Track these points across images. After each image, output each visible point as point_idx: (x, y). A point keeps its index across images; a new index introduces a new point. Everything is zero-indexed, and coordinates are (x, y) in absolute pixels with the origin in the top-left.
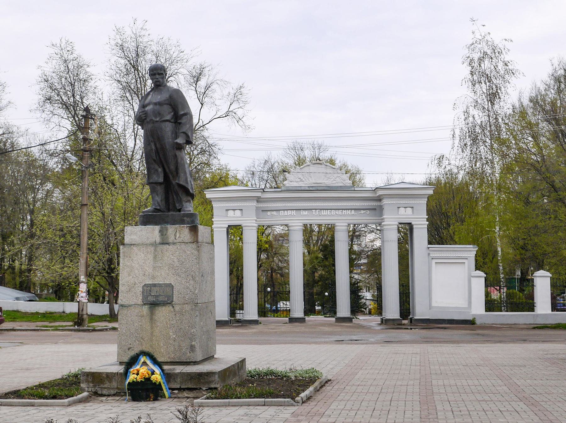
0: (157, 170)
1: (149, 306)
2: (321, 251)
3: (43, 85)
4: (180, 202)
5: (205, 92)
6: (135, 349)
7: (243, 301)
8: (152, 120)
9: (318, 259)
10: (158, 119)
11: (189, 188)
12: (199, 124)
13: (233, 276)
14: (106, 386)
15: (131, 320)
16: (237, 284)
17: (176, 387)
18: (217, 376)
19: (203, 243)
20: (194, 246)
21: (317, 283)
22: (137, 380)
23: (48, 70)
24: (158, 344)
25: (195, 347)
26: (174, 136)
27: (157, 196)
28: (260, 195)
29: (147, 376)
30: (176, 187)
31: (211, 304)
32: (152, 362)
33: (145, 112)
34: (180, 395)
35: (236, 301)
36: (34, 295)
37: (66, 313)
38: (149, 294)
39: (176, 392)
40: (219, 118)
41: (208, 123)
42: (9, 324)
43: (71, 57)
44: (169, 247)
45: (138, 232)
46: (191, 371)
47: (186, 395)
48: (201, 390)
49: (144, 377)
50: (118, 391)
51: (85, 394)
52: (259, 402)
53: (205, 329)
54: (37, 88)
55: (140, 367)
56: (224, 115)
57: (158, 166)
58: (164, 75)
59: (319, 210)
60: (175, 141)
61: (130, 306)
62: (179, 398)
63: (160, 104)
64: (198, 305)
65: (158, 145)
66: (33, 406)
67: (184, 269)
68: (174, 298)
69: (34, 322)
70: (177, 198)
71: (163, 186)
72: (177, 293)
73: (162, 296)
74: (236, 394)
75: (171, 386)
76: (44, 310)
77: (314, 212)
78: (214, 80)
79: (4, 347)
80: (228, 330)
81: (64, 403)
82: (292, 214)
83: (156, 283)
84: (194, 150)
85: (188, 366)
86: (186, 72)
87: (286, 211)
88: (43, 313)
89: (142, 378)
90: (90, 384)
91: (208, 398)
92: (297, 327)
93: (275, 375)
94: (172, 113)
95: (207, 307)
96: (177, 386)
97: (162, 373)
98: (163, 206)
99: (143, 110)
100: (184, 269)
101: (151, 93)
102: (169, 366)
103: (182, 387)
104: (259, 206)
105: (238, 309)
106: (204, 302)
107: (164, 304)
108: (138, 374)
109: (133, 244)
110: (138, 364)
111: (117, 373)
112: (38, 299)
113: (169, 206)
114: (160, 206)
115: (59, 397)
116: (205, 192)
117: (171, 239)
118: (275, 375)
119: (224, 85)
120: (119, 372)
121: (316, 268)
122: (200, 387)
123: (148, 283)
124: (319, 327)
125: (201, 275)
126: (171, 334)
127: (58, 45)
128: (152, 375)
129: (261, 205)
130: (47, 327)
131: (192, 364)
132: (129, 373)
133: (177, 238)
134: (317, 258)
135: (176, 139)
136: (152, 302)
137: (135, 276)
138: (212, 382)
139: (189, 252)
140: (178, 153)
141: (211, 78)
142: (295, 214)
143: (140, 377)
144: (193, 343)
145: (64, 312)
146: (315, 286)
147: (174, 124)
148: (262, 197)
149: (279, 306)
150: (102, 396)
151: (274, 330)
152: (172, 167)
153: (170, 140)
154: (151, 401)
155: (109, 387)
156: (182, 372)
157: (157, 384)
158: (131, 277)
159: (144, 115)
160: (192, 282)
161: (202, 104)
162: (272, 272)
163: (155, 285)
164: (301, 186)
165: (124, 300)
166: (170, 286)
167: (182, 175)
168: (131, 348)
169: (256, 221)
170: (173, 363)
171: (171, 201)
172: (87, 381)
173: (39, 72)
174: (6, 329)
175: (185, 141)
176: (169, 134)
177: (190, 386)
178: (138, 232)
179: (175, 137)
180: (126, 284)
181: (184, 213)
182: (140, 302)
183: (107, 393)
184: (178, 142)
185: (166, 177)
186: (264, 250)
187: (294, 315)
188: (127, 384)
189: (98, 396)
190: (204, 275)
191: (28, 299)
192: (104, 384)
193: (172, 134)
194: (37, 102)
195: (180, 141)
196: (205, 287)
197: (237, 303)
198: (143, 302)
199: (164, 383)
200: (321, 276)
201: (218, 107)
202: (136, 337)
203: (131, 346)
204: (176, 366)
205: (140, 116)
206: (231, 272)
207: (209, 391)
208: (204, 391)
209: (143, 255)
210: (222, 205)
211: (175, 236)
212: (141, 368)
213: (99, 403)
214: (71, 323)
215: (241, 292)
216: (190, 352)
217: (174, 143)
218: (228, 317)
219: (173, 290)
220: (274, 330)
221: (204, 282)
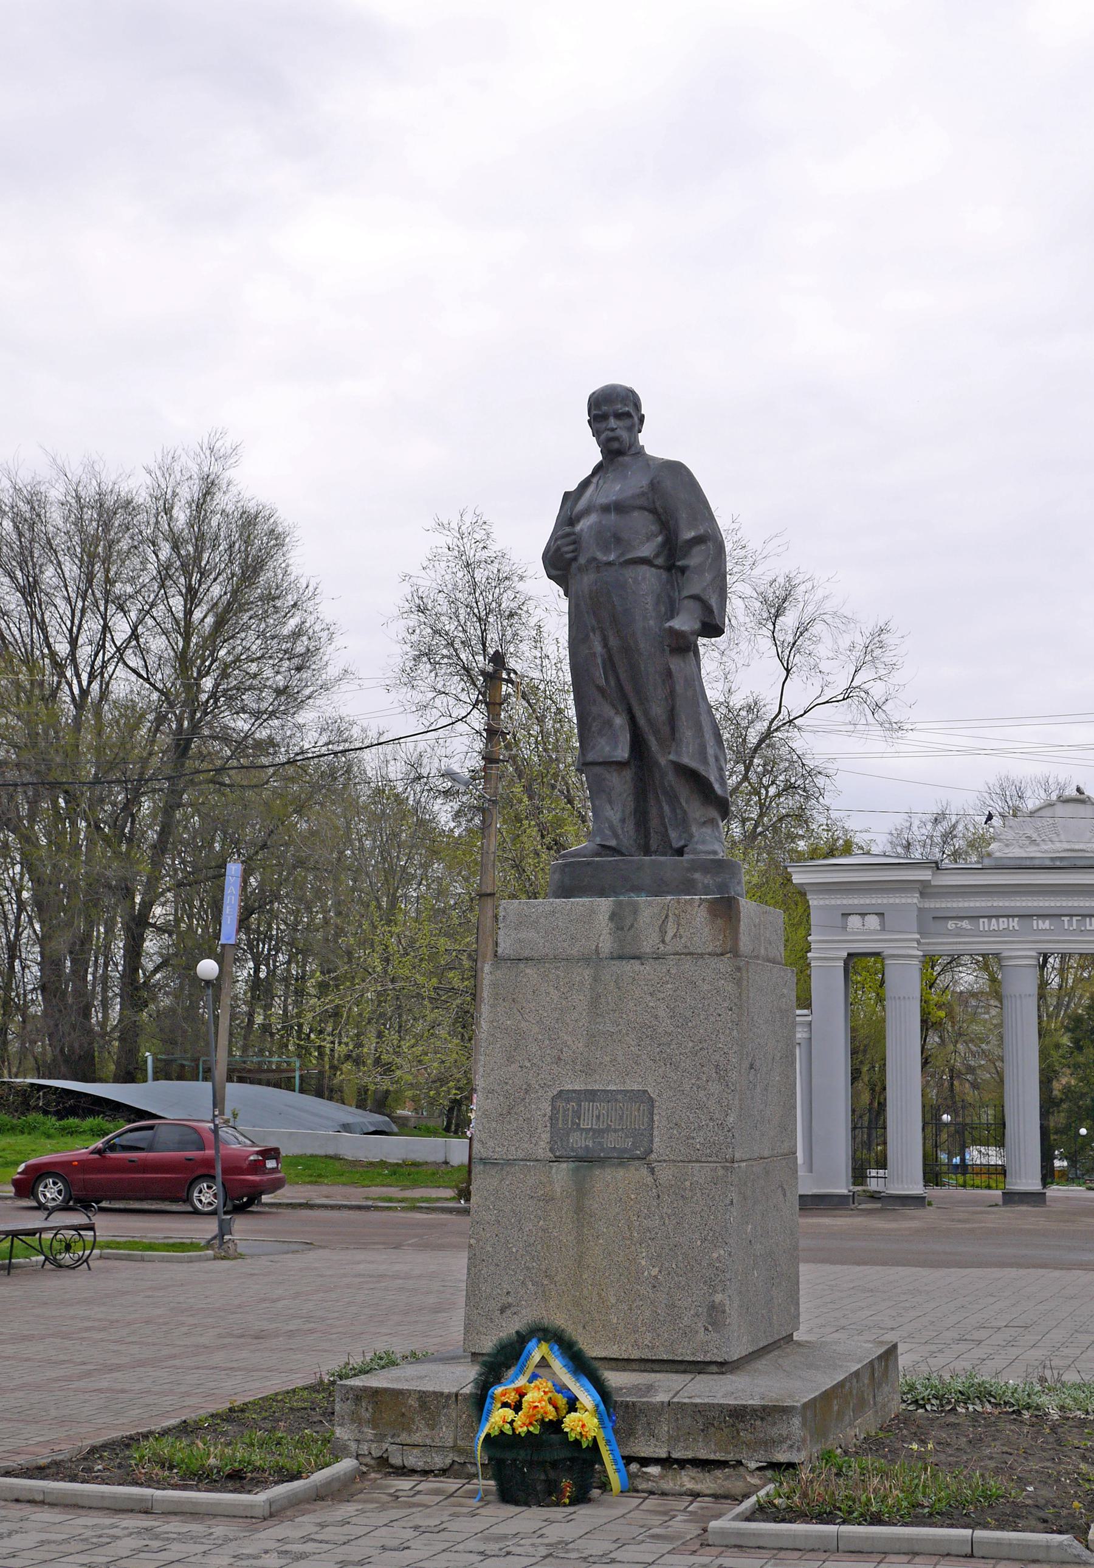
0: (609, 723)
1: (572, 1165)
2: (1068, 1029)
3: (414, 619)
4: (683, 823)
5: (796, 642)
6: (524, 1312)
7: (885, 1143)
8: (595, 559)
9: (1059, 1048)
10: (612, 557)
11: (712, 779)
12: (781, 717)
13: (861, 1084)
14: (417, 1438)
15: (514, 1211)
16: (871, 1104)
17: (655, 1456)
18: (796, 1421)
19: (757, 957)
20: (724, 965)
21: (1058, 1105)
22: (513, 1429)
23: (428, 583)
24: (599, 1295)
25: (724, 1312)
26: (663, 609)
27: (608, 807)
28: (929, 878)
29: (552, 1415)
30: (671, 777)
31: (784, 1162)
32: (571, 1364)
33: (573, 537)
34: (667, 1485)
35: (868, 1145)
36: (387, 1119)
37: (452, 1166)
38: (573, 1123)
39: (654, 1470)
40: (827, 702)
41: (801, 716)
42: (302, 1189)
43: (483, 555)
44: (642, 968)
45: (542, 920)
46: (706, 1401)
47: (689, 1485)
48: (741, 1469)
49: (539, 1417)
50: (456, 1459)
51: (346, 1465)
52: (949, 1540)
53: (759, 1246)
54: (399, 627)
55: (530, 1381)
56: (841, 697)
57: (613, 706)
58: (636, 419)
59: (1079, 918)
60: (667, 625)
61: (510, 1162)
62: (664, 1494)
63: (619, 507)
64: (736, 1165)
65: (613, 642)
66: (146, 1512)
67: (691, 1044)
68: (656, 1140)
69: (363, 1187)
70: (673, 811)
71: (628, 774)
72: (664, 1123)
73: (615, 1131)
74: (864, 1498)
75: (635, 1449)
76: (400, 1157)
77: (1066, 922)
78: (818, 612)
79: (252, 1256)
80: (849, 1220)
81: (252, 1506)
82: (1011, 928)
83: (596, 1087)
84: (769, 786)
85: (699, 1377)
86: (749, 591)
87: (994, 920)
88: (397, 1164)
89: (531, 1424)
90: (366, 1430)
91: (762, 1512)
92: (1024, 1216)
93: (993, 1400)
94: (660, 539)
95: (767, 1173)
96: (657, 1450)
97: (602, 1407)
98: (627, 835)
99: (567, 529)
100: (691, 1044)
101: (595, 480)
102: (634, 1374)
103: (675, 1455)
104: (927, 905)
105: (873, 1163)
106: (756, 1155)
107: (623, 1159)
108: (517, 1408)
109: (526, 959)
110: (521, 1371)
111: (457, 1395)
112: (395, 1129)
113: (647, 836)
114: (616, 835)
115: (255, 1475)
116: (789, 870)
117: (649, 943)
118: (993, 1400)
119: (841, 626)
120: (461, 1392)
121: (1056, 1071)
122: (738, 1457)
123: (569, 1087)
124: (1083, 1219)
125: (746, 1064)
126: (643, 1263)
127: (454, 525)
128: (568, 1412)
129: (931, 904)
130: (390, 1200)
131: (714, 1368)
132: (488, 1400)
133: (668, 939)
134: (1058, 1046)
135: (672, 617)
136: (581, 1153)
137: (528, 1065)
138: (782, 1440)
139: (706, 987)
140: (676, 664)
141: (810, 608)
142: (1017, 928)
143: (524, 1419)
144: (718, 1298)
145: (446, 1163)
146: (1053, 1113)
147: (664, 575)
148: (933, 883)
149: (967, 1157)
150: (404, 1474)
151: (967, 1226)
152: (658, 710)
153: (652, 622)
154: (565, 1505)
155: (428, 1442)
156: (675, 1400)
157: (584, 1446)
158: (514, 1067)
159: (571, 548)
160: (715, 1087)
161: (788, 671)
162: (952, 1077)
163: (592, 1095)
164: (1032, 858)
165: (491, 1143)
166: (643, 1098)
167: (687, 733)
168: (510, 1305)
169: (919, 942)
170: (649, 1366)
171: (654, 823)
172: (355, 1419)
173: (406, 589)
174: (291, 1204)
175: (697, 626)
176: (649, 602)
177: (703, 1454)
178: (542, 920)
179: (666, 613)
180: (496, 1087)
181: (693, 860)
182: (542, 1150)
183: (421, 1465)
184: (677, 627)
185: (638, 744)
186: (933, 1024)
187: (1015, 1184)
188: (481, 1439)
189: (389, 1474)
190: (757, 1064)
191: (372, 1129)
192: (410, 1432)
193: (657, 604)
194: (399, 661)
195: (683, 623)
196: (761, 1107)
197: (869, 1150)
198: (551, 1150)
199: (608, 1442)
200: (1067, 1090)
201: (826, 678)
202: (528, 1269)
203: (510, 1300)
204: (659, 1376)
205: (558, 549)
206: (855, 1075)
207: (769, 1473)
208: (752, 1472)
209: (555, 994)
210: (833, 902)
211: (663, 931)
212: (532, 1385)
213: (383, 1507)
214: (450, 1193)
215: (881, 1122)
216: (706, 1329)
217: (665, 630)
218: (847, 1186)
219: (652, 1114)
220: (967, 1226)
221: (758, 1090)
